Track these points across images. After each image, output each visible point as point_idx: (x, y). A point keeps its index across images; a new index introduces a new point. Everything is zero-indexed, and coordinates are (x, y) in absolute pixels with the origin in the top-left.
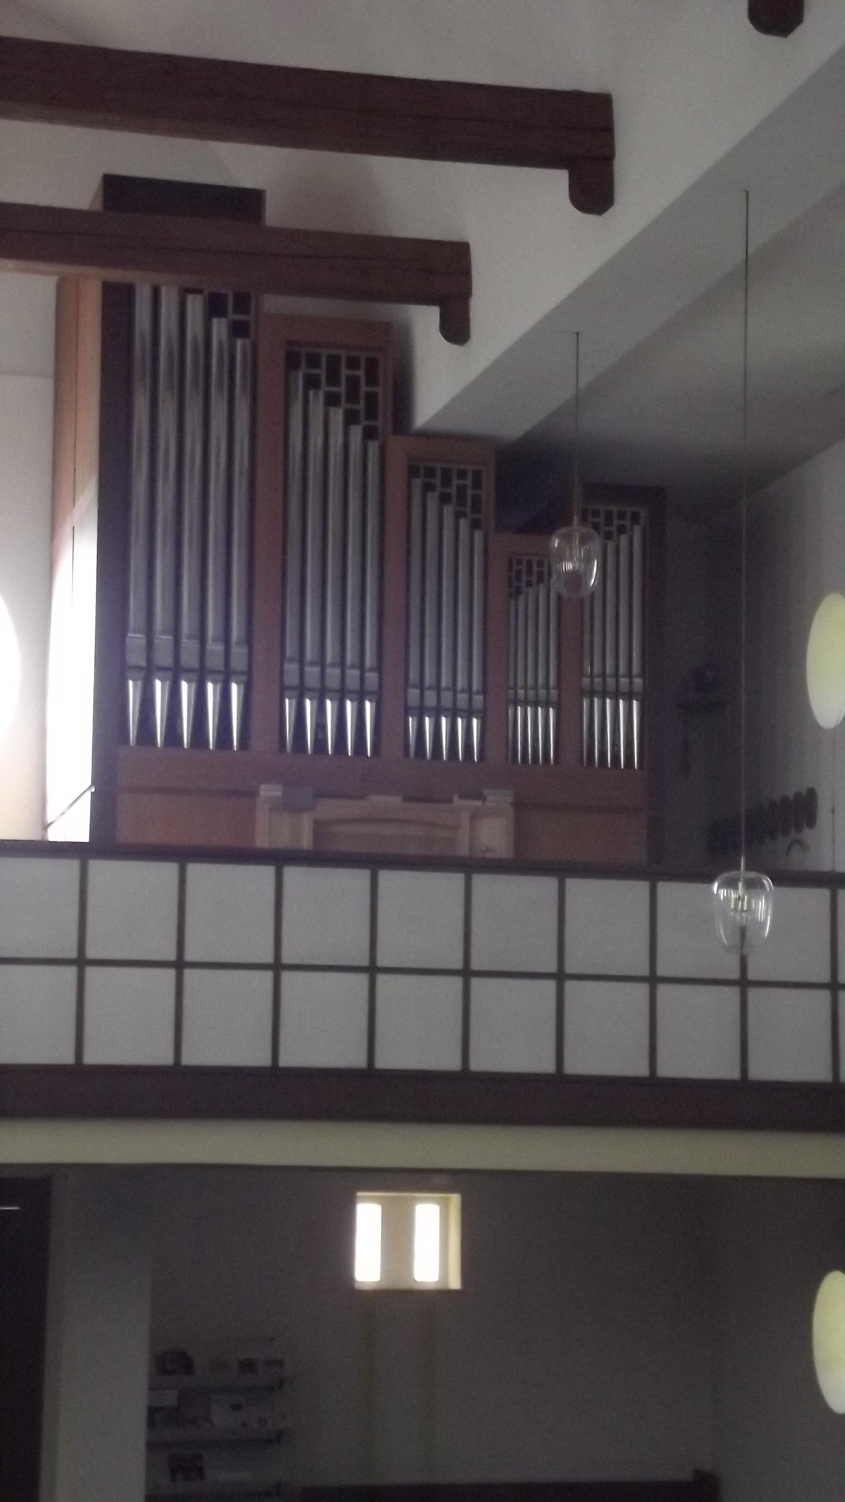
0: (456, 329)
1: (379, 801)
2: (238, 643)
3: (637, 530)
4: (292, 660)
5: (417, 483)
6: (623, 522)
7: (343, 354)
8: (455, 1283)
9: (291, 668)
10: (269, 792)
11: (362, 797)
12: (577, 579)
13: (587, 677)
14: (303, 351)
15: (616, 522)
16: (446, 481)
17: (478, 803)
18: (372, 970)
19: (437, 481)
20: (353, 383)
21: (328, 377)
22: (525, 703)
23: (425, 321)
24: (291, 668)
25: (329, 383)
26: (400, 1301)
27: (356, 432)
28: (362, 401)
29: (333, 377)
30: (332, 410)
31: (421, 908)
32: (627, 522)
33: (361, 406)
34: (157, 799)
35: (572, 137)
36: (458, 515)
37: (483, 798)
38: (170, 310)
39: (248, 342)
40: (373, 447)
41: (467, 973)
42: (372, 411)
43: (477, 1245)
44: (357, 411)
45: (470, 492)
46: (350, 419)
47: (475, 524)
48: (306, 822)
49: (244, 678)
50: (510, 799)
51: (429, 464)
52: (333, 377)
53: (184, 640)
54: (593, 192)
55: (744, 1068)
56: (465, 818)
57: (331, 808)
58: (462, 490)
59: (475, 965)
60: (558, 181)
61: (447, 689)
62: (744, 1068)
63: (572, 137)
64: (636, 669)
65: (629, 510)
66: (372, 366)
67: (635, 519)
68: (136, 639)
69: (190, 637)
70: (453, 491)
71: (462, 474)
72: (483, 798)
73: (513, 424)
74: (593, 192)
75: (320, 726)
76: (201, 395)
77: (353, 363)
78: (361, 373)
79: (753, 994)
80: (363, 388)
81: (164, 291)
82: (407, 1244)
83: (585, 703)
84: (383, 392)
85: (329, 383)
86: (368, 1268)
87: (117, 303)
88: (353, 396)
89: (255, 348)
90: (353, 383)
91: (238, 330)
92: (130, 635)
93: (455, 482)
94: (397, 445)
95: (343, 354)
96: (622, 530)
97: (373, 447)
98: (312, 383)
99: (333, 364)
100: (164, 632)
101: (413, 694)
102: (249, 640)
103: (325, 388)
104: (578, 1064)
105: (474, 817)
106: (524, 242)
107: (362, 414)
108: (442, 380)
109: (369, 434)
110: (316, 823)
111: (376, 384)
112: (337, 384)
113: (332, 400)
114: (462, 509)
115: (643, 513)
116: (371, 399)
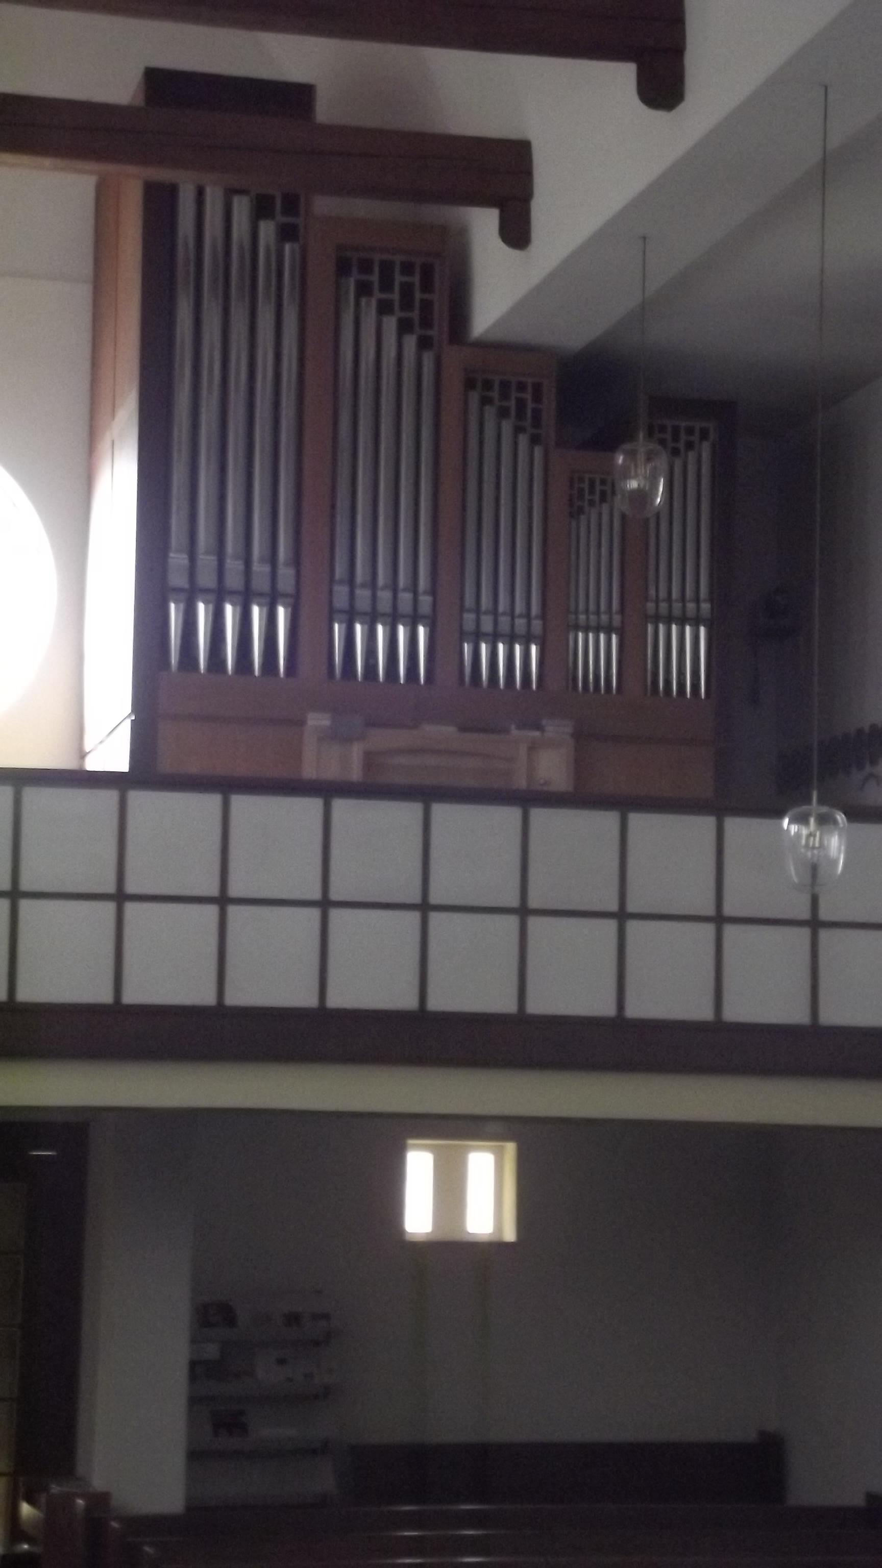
0: (517, 233)
3: (706, 450)
8: (510, 1235)
12: (642, 497)
23: (483, 224)
38: (217, 212)
41: (523, 911)
42: (426, 322)
54: (662, 87)
60: (624, 75)
73: (575, 332)
74: (662, 87)
82: (460, 1193)
86: (418, 1218)
91: (287, 233)
98: (364, 289)
108: (501, 287)
109: (424, 343)
111: (432, 290)
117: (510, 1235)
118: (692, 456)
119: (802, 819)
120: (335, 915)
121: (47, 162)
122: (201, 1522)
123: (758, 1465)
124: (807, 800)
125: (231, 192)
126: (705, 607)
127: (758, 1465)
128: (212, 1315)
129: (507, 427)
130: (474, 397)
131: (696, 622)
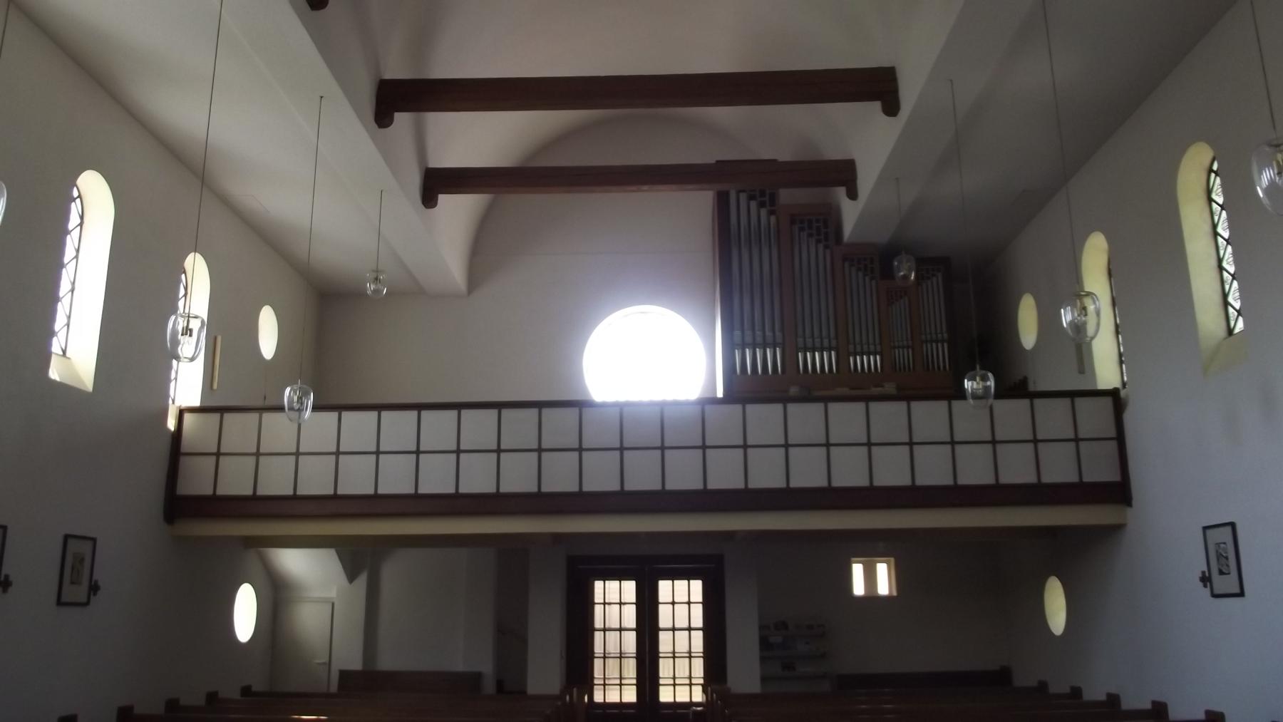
0: (853, 195)
3: (940, 275)
8: (895, 593)
9: (800, 340)
12: (906, 277)
18: (828, 445)
23: (841, 192)
24: (800, 340)
26: (871, 598)
31: (847, 418)
34: (744, 389)
35: (878, 87)
38: (747, 213)
41: (869, 444)
42: (826, 239)
43: (901, 577)
54: (892, 108)
55: (997, 479)
59: (873, 441)
60: (877, 105)
62: (997, 479)
63: (878, 87)
73: (881, 236)
74: (892, 108)
79: (999, 447)
82: (873, 579)
86: (859, 589)
87: (722, 202)
89: (778, 221)
91: (771, 213)
98: (802, 229)
101: (851, 347)
104: (922, 481)
106: (865, 137)
108: (851, 214)
109: (826, 247)
111: (824, 224)
117: (895, 593)
118: (934, 279)
119: (973, 379)
120: (791, 450)
121: (674, 187)
122: (362, 684)
123: (1002, 677)
124: (974, 369)
125: (739, 192)
126: (946, 335)
127: (1002, 677)
128: (762, 628)
129: (860, 274)
130: (847, 264)
131: (943, 341)
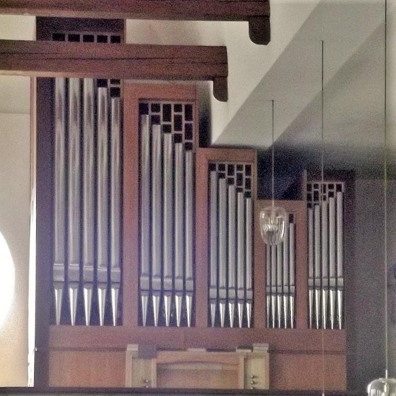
1: (193, 352)
2: (115, 266)
3: (339, 196)
4: (145, 275)
5: (214, 175)
6: (332, 191)
7: (172, 104)
9: (145, 279)
10: (132, 348)
11: (185, 350)
13: (311, 278)
14: (150, 103)
15: (328, 190)
16: (231, 171)
17: (249, 351)
19: (226, 172)
20: (178, 120)
21: (175, 127)
22: (276, 294)
25: (175, 129)
27: (180, 147)
28: (173, 120)
29: (167, 117)
30: (177, 145)
32: (334, 190)
33: (183, 132)
36: (238, 190)
37: (252, 348)
39: (118, 99)
40: (189, 155)
42: (189, 135)
44: (170, 126)
45: (245, 177)
46: (177, 139)
47: (247, 195)
48: (153, 364)
49: (118, 286)
50: (267, 349)
51: (154, 102)
52: (167, 117)
53: (99, 267)
56: (242, 360)
57: (165, 356)
58: (240, 177)
61: (325, 277)
64: (339, 273)
65: (335, 183)
66: (189, 109)
67: (339, 188)
68: (58, 267)
69: (103, 265)
70: (235, 177)
71: (240, 168)
72: (252, 348)
75: (173, 310)
76: (93, 127)
77: (178, 108)
78: (183, 114)
80: (184, 122)
81: (85, 80)
83: (310, 292)
84: (195, 123)
85: (164, 120)
88: (178, 127)
90: (178, 120)
91: (115, 92)
92: (55, 264)
93: (236, 172)
94: (204, 155)
95: (172, 104)
96: (331, 195)
97: (189, 155)
99: (167, 108)
100: (74, 262)
101: (311, 281)
102: (121, 264)
103: (173, 132)
105: (246, 360)
107: (162, 118)
109: (188, 147)
110: (158, 364)
112: (180, 129)
113: (166, 129)
114: (222, 172)
115: (343, 184)
116: (189, 128)
